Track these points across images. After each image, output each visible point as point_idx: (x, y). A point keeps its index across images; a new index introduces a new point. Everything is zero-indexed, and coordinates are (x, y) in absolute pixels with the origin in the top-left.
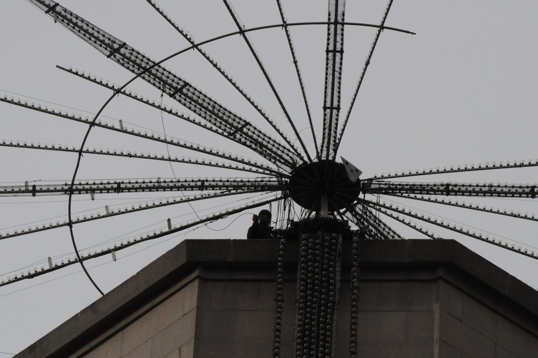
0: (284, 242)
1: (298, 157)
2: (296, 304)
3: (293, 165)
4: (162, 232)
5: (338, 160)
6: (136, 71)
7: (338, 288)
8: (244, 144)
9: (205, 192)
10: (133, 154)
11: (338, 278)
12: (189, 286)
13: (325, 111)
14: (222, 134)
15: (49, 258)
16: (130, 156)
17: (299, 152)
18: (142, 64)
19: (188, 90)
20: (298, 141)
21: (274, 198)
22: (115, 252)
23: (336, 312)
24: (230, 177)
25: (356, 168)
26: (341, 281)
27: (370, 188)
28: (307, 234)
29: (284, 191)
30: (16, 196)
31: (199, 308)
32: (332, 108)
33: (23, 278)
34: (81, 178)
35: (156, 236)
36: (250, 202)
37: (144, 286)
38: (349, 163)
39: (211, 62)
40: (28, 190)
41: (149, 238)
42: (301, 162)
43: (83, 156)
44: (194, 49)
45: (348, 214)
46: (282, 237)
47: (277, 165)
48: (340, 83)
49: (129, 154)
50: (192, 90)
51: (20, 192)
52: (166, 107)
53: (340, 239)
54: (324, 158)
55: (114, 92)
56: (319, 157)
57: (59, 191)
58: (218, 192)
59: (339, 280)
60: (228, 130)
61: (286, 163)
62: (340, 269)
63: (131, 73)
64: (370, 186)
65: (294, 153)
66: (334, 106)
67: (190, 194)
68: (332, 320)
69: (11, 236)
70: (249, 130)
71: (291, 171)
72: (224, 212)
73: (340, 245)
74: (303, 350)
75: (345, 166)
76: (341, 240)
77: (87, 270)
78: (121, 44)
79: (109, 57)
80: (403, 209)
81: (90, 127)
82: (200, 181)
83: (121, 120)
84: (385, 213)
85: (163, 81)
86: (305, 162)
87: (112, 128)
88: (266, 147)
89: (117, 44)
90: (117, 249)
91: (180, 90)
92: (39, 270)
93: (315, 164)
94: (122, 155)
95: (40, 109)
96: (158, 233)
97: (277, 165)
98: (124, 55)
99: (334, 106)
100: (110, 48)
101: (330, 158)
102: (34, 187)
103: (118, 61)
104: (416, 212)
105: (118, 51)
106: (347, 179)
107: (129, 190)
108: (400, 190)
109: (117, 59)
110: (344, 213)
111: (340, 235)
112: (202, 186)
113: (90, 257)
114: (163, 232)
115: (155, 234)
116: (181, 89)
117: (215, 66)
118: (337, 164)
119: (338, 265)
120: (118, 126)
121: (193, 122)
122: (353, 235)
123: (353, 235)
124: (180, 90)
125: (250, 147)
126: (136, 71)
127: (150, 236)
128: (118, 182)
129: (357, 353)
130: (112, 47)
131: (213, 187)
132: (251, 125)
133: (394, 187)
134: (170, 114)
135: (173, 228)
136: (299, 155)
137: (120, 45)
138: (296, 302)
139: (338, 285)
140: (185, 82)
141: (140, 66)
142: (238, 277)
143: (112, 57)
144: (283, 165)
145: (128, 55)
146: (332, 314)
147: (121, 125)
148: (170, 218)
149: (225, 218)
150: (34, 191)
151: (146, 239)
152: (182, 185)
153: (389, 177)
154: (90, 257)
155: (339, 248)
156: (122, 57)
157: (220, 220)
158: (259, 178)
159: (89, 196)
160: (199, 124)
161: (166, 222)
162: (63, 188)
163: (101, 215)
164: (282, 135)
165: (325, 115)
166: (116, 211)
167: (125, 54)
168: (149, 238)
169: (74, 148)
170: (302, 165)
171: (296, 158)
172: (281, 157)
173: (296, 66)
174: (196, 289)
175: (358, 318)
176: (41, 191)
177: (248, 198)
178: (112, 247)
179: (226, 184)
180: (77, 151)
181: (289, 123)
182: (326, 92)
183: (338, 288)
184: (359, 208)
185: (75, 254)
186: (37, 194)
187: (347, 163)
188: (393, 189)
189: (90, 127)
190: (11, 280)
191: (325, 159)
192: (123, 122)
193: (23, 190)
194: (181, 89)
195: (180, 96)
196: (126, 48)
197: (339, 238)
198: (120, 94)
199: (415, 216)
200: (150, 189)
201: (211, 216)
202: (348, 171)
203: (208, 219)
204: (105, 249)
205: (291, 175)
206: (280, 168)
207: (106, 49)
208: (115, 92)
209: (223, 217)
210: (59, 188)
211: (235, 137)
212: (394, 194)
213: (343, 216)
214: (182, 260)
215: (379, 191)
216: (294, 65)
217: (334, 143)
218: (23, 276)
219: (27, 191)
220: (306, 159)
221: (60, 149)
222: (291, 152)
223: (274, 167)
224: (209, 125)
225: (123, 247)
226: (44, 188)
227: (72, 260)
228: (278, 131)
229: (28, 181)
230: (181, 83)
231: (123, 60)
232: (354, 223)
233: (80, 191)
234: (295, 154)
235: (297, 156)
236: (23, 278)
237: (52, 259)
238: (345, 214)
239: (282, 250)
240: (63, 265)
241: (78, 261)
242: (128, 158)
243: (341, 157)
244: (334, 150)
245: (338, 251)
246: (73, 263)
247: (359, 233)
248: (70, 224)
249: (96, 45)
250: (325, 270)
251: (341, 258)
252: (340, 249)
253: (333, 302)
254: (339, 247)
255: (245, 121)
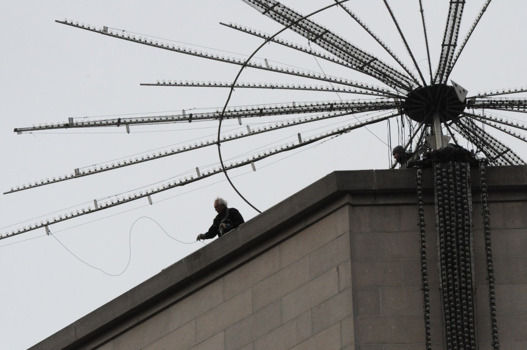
0: (421, 172)
1: (415, 82)
2: (436, 227)
3: (409, 89)
4: (293, 145)
5: (449, 84)
6: (285, 22)
7: (471, 212)
8: (370, 74)
9: (332, 113)
10: (275, 86)
11: (470, 203)
12: (340, 211)
13: (443, 47)
14: (351, 67)
15: (197, 168)
16: (272, 87)
17: (415, 78)
18: (291, 18)
19: (328, 36)
20: (417, 70)
21: (391, 114)
22: (254, 163)
23: (471, 234)
24: (354, 99)
25: (463, 88)
26: (473, 202)
27: (475, 104)
28: (440, 163)
29: (400, 109)
30: (175, 123)
31: (351, 232)
32: (449, 45)
33: (176, 185)
34: (231, 107)
35: (288, 149)
36: (370, 118)
37: (298, 210)
38: (466, 90)
39: (350, 14)
40: (186, 118)
41: (283, 150)
42: (417, 86)
43: (234, 91)
44: (337, 5)
45: (454, 125)
46: (418, 167)
47: (397, 90)
48: (459, 26)
49: (271, 86)
50: (330, 35)
51: (179, 120)
52: (306, 49)
53: (469, 167)
54: (437, 83)
55: (266, 40)
56: (433, 82)
57: (211, 118)
58: (344, 112)
59: (471, 205)
60: (357, 64)
61: (404, 87)
62: (471, 195)
63: (281, 25)
64: (474, 103)
65: (412, 80)
66: (452, 44)
67: (320, 114)
68: (469, 241)
69: (169, 155)
70: (375, 63)
71: (407, 93)
72: (347, 127)
73: (469, 172)
74: (447, 270)
75: (455, 88)
76: (469, 168)
77: (230, 179)
78: (275, 4)
79: (264, 13)
80: (501, 119)
81: (243, 68)
82: (329, 104)
83: (266, 59)
84: (490, 124)
85: (307, 30)
86: (420, 86)
87: (260, 68)
88: (388, 76)
89: (272, 4)
90: (255, 160)
91: (321, 37)
92: (189, 179)
93: (429, 87)
94: (266, 87)
95: (201, 55)
96: (290, 146)
97: (397, 89)
98: (276, 12)
99: (452, 44)
100: (265, 6)
101: (443, 83)
102: (191, 115)
103: (272, 16)
104: (512, 121)
105: (272, 9)
106: (457, 98)
107: (269, 114)
108: (500, 105)
109: (270, 15)
110: (451, 124)
111: (468, 164)
112: (331, 108)
113: (232, 167)
114: (295, 145)
115: (287, 147)
116: (322, 35)
117: (353, 16)
118: (449, 87)
119: (468, 191)
120: (264, 66)
121: (328, 59)
122: (479, 163)
123: (479, 163)
124: (321, 37)
125: (375, 77)
126: (285, 22)
127: (283, 148)
128: (260, 108)
129: (493, 271)
130: (267, 6)
131: (340, 109)
132: (377, 60)
133: (495, 103)
134: (310, 55)
135: (303, 142)
136: (415, 81)
137: (274, 4)
138: (436, 226)
139: (471, 210)
140: (325, 29)
141: (289, 19)
142: (382, 202)
143: (267, 13)
144: (401, 89)
145: (280, 11)
146: (468, 236)
147: (267, 64)
148: (300, 133)
149: (348, 132)
150: (191, 118)
151: (280, 152)
152: (314, 108)
153: (492, 94)
154: (232, 167)
155: (468, 176)
156: (274, 13)
157: (344, 134)
158: (378, 99)
159: (236, 120)
160: (333, 61)
161: (297, 136)
162: (214, 115)
163: (244, 134)
164: (402, 65)
165: (443, 51)
166: (256, 131)
167: (277, 11)
168: (283, 150)
169: (226, 83)
170: (417, 88)
171: (412, 83)
172: (400, 83)
173: (422, 15)
174: (347, 213)
175: (491, 239)
176: (197, 118)
177: (368, 115)
178: (251, 159)
179: (351, 105)
180: (229, 87)
181: (410, 57)
182: (446, 33)
183: (471, 212)
184: (463, 120)
185: (220, 164)
186: (192, 121)
187: (456, 85)
188: (493, 104)
189: (243, 68)
190: (166, 187)
191: (439, 83)
192: (268, 61)
193: (182, 118)
194: (322, 35)
195: (320, 41)
196: (279, 7)
197: (467, 167)
198: (270, 41)
199: (511, 125)
200: (287, 113)
201: (336, 131)
202: (458, 92)
203: (333, 134)
204: (245, 161)
205: (407, 97)
206: (399, 91)
207: (262, 7)
208: (266, 40)
209: (347, 131)
210: (211, 115)
211: (363, 69)
212: (494, 108)
213: (449, 126)
214: (333, 189)
215: (484, 106)
216: (421, 13)
217: (447, 71)
218: (175, 184)
219: (184, 119)
220: (421, 83)
221: (215, 86)
222: (409, 79)
223: (393, 91)
224: (341, 61)
225: (260, 158)
226: (199, 116)
227: (217, 170)
228: (399, 63)
229: (184, 110)
230: (322, 31)
231: (275, 15)
232: (458, 132)
233: (228, 117)
234: (412, 81)
235: (414, 82)
236: (176, 185)
237: (199, 169)
238: (451, 125)
239: (419, 179)
240: (210, 175)
241: (223, 171)
242: (271, 89)
243: (451, 80)
244: (446, 76)
245: (467, 178)
246: (218, 172)
247: (484, 161)
248: (218, 143)
249: (254, 5)
250: (459, 197)
251: (471, 184)
252: (469, 176)
253: (468, 226)
254: (468, 174)
255: (373, 57)
